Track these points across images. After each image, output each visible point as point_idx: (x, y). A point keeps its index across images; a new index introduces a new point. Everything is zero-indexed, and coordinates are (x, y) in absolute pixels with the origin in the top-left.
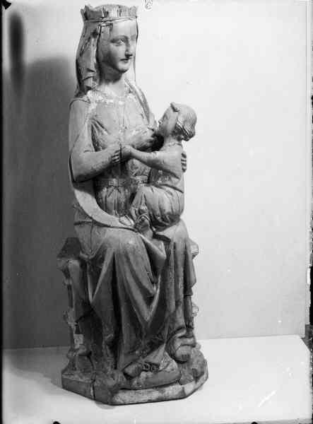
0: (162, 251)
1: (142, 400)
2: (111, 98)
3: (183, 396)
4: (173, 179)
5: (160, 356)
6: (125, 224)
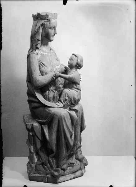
1: (68, 179)
2: (46, 53)
4: (77, 85)
5: (74, 160)
6: (59, 106)
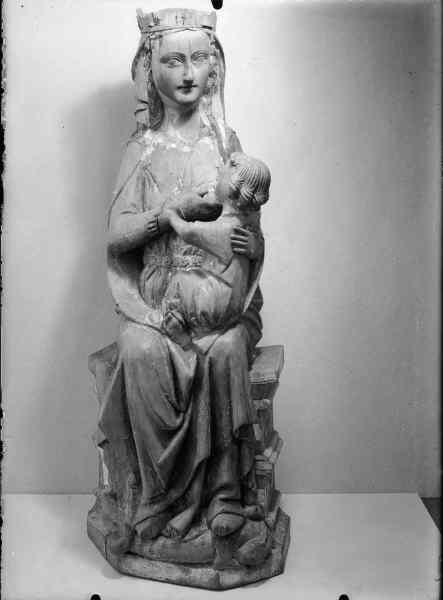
0: (188, 365)
3: (218, 587)
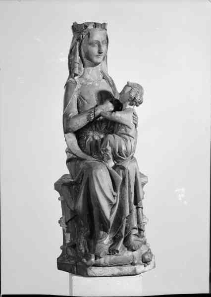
2: (91, 82)
3: (134, 274)
